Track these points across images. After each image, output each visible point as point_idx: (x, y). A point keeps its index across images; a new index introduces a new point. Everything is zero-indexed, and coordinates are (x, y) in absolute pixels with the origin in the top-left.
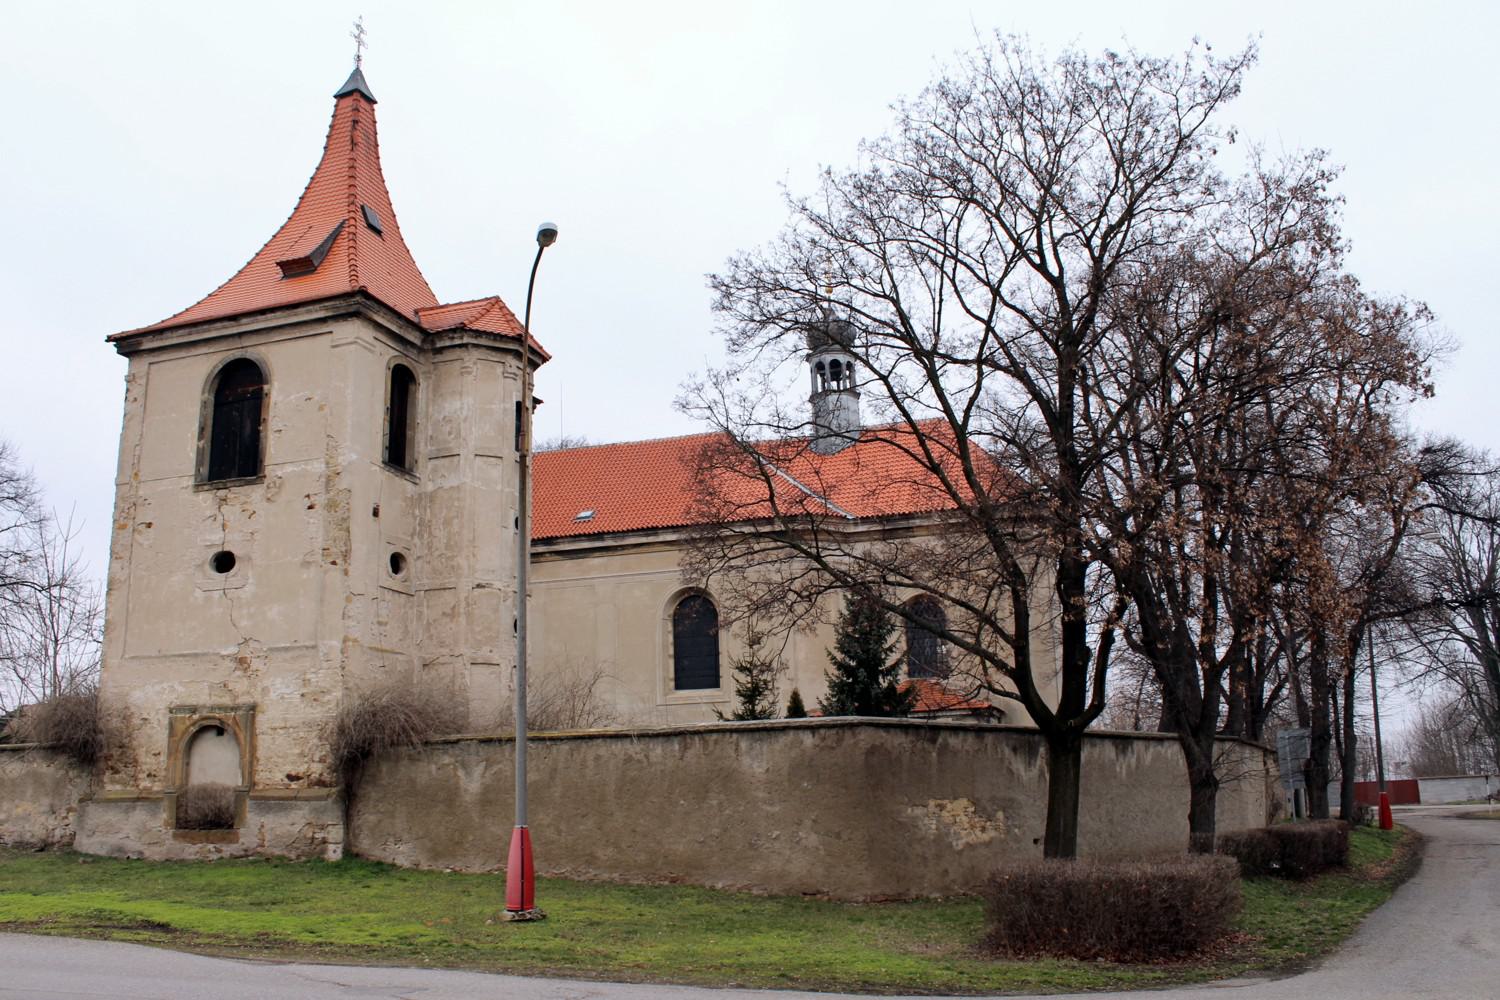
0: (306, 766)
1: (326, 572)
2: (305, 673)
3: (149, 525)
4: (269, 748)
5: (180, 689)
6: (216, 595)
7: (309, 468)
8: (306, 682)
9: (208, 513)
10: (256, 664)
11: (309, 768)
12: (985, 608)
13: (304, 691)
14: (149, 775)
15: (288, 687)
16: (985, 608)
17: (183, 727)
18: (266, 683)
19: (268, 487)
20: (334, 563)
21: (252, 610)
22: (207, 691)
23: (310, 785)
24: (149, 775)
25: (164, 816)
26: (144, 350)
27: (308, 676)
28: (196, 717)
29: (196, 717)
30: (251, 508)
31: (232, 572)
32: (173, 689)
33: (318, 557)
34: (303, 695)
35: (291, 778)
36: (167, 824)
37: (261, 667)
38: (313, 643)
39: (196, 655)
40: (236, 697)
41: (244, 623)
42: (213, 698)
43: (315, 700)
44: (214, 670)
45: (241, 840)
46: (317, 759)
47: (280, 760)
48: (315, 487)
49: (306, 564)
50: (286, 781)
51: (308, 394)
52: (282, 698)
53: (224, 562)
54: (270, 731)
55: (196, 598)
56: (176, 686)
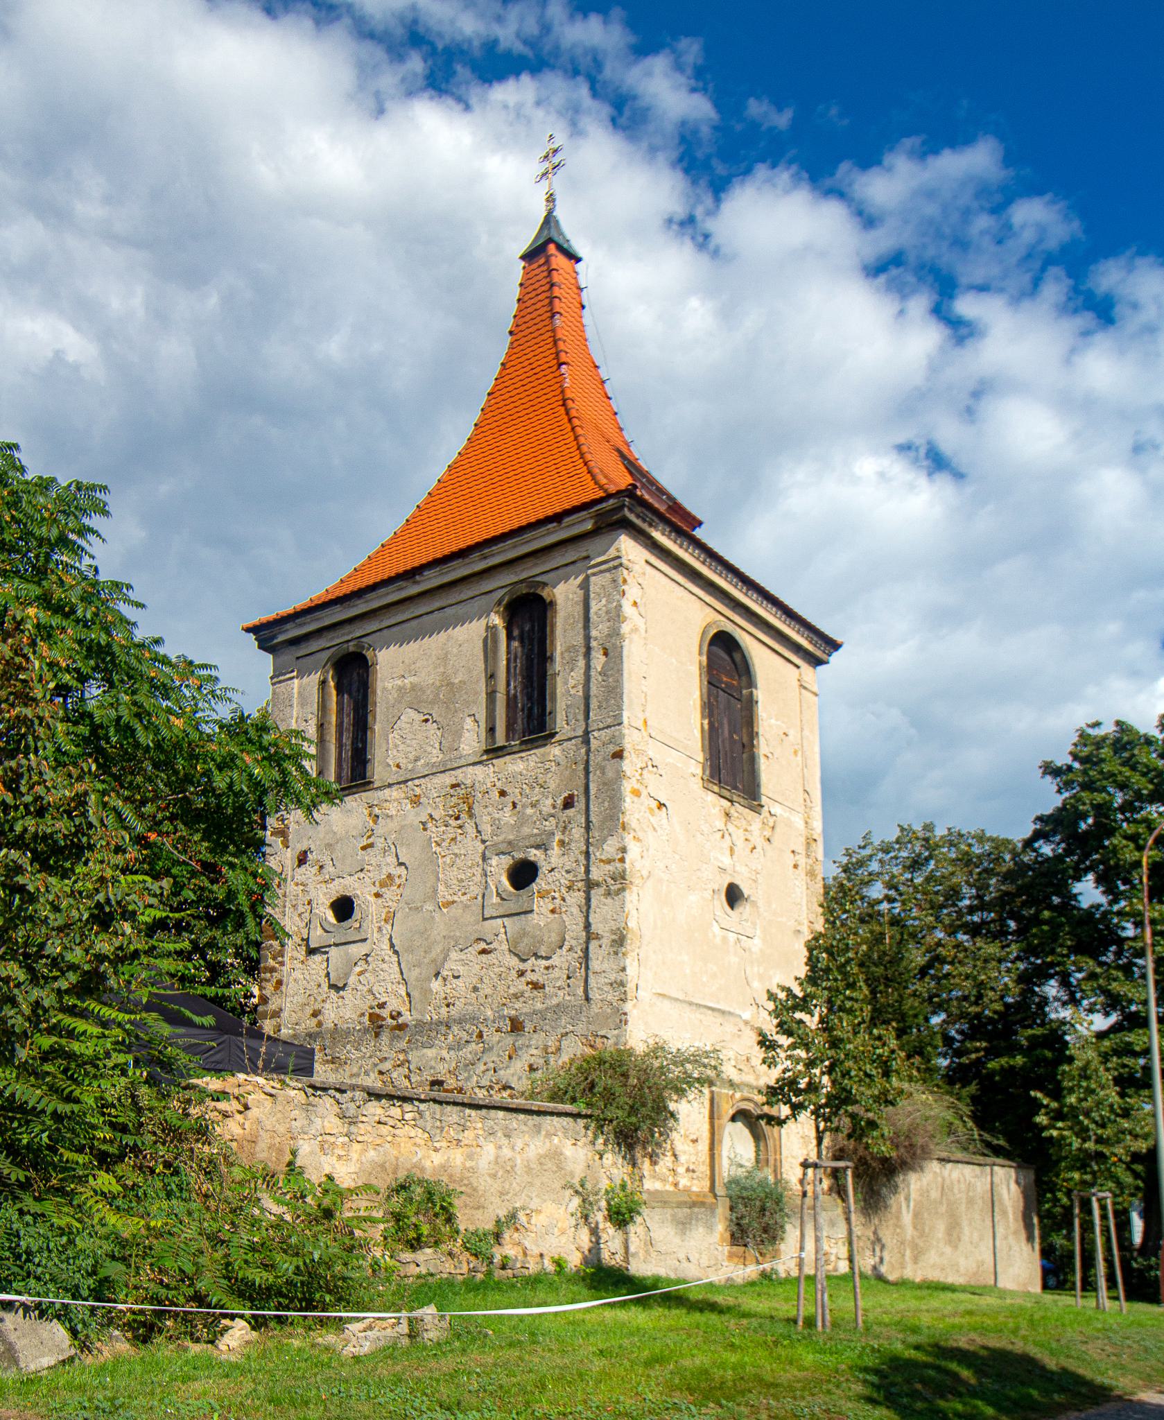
7: (792, 819)
26: (650, 538)
39: (723, 1012)
44: (739, 1036)
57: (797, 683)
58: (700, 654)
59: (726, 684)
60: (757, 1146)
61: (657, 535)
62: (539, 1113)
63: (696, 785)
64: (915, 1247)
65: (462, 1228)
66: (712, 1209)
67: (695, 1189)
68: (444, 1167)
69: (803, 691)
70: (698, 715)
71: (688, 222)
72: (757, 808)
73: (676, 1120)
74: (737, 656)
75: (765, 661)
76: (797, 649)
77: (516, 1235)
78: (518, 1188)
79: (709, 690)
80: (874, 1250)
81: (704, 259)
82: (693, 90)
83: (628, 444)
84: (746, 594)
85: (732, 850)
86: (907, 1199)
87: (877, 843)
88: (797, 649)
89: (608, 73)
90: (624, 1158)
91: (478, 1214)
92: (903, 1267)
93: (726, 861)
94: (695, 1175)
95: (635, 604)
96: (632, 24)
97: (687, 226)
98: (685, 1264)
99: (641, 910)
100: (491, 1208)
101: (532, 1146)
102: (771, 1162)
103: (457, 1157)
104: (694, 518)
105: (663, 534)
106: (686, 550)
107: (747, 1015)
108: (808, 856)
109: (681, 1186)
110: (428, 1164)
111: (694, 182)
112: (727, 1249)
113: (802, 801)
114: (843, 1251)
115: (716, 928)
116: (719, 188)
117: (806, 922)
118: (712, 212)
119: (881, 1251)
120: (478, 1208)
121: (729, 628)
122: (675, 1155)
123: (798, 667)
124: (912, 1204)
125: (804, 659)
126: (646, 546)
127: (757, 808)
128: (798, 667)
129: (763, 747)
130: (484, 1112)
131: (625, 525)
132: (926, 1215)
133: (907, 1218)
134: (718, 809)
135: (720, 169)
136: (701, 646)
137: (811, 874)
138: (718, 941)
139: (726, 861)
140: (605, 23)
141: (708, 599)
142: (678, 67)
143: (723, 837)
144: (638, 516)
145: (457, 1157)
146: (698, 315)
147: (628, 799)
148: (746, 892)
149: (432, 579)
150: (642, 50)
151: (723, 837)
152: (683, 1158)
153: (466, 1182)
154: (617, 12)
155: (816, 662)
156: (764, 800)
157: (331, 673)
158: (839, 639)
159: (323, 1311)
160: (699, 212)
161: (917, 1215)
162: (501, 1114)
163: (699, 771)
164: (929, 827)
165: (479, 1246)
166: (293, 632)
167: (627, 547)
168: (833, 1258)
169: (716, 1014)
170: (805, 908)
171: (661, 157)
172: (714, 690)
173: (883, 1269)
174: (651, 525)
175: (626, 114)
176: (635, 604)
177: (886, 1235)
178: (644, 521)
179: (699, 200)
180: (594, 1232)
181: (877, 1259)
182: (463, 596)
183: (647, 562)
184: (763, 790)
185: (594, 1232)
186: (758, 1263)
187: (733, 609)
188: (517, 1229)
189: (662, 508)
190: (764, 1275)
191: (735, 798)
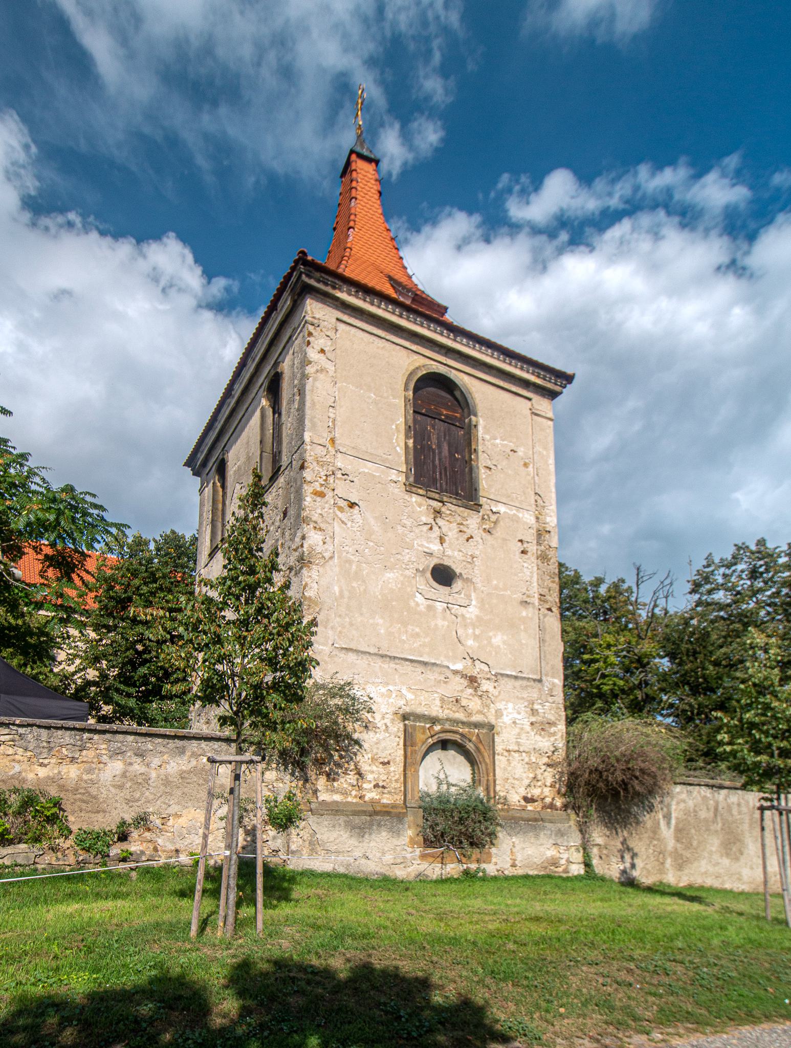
0: (539, 790)
1: (545, 616)
2: (533, 704)
3: (352, 505)
4: (505, 769)
5: (410, 696)
6: (440, 606)
7: (520, 515)
8: (534, 712)
9: (424, 519)
10: (486, 686)
11: (542, 792)
12: (766, 882)
13: (533, 719)
14: (376, 786)
15: (519, 713)
16: (766, 882)
17: (423, 737)
18: (500, 705)
19: (483, 519)
20: (550, 609)
21: (477, 632)
22: (438, 703)
23: (545, 807)
24: (376, 786)
25: (410, 833)
26: (337, 299)
27: (536, 707)
28: (437, 728)
29: (437, 728)
30: (469, 532)
31: (435, 585)
32: (400, 695)
33: (536, 601)
34: (532, 724)
35: (526, 799)
36: (412, 842)
37: (491, 689)
38: (537, 677)
39: (425, 664)
40: (470, 714)
41: (470, 642)
42: (446, 711)
43: (543, 729)
44: (445, 683)
45: (494, 860)
46: (548, 784)
47: (516, 782)
48: (530, 536)
49: (525, 603)
50: (523, 803)
51: (512, 446)
52: (514, 722)
53: (443, 575)
54: (506, 754)
55: (417, 604)
56: (404, 691)
57: (529, 412)
58: (406, 389)
59: (447, 416)
60: (473, 770)
61: (339, 294)
62: (690, 785)
63: (398, 490)
64: (676, 855)
65: (74, 828)
66: (400, 817)
67: (385, 801)
68: (52, 780)
69: (535, 418)
70: (402, 436)
71: (733, 262)
72: (477, 507)
73: (361, 746)
74: (457, 393)
75: (481, 393)
76: (526, 384)
77: (147, 834)
78: (151, 797)
79: (415, 421)
80: (622, 857)
81: (743, 283)
82: (733, 185)
83: (410, 277)
84: (455, 340)
85: (441, 538)
86: (668, 817)
87: (717, 561)
88: (526, 384)
89: (677, 197)
90: (292, 774)
91: (100, 817)
92: (662, 871)
93: (435, 547)
94: (386, 791)
95: (322, 351)
96: (692, 164)
97: (734, 267)
98: (363, 861)
99: (321, 583)
100: (114, 813)
101: (172, 764)
102: (484, 780)
103: (72, 772)
104: (439, 305)
105: (350, 295)
106: (379, 307)
107: (459, 666)
108: (539, 544)
109: (367, 799)
110: (31, 776)
111: (735, 239)
112: (418, 851)
113: (533, 502)
114: (578, 857)
115: (419, 599)
116: (752, 237)
117: (536, 596)
118: (747, 253)
119: (632, 858)
120: (98, 812)
121: (442, 370)
122: (360, 774)
123: (530, 399)
124: (673, 822)
125: (536, 393)
126: (337, 308)
127: (477, 507)
128: (530, 399)
129: (482, 461)
130: (108, 736)
131: (307, 290)
132: (693, 831)
133: (667, 833)
134: (424, 508)
135: (752, 225)
136: (406, 385)
137: (543, 557)
138: (422, 608)
139: (435, 547)
140: (675, 170)
141: (414, 347)
142: (724, 175)
143: (431, 528)
144: (318, 281)
145: (72, 772)
146: (739, 315)
147: (308, 499)
148: (458, 571)
149: (238, 389)
150: (699, 173)
151: (431, 528)
152: (370, 777)
153: (82, 791)
154: (683, 160)
155: (552, 395)
156: (482, 501)
157: (217, 477)
158: (569, 371)
159: (265, 889)
160: (739, 255)
161: (679, 830)
162: (131, 738)
163: (402, 478)
164: (761, 542)
165: (93, 843)
166: (201, 457)
167: (313, 308)
168: (563, 862)
169: (416, 665)
170: (535, 584)
171: (714, 233)
172: (419, 417)
173: (635, 874)
174: (334, 288)
175: (688, 217)
176: (322, 351)
177: (638, 845)
178: (326, 284)
179: (738, 248)
180: (251, 832)
181: (628, 865)
182: (253, 395)
183: (338, 319)
184: (481, 493)
185: (251, 832)
186: (460, 861)
187: (446, 355)
188: (149, 830)
189: (408, 302)
190: (466, 873)
191: (445, 499)
